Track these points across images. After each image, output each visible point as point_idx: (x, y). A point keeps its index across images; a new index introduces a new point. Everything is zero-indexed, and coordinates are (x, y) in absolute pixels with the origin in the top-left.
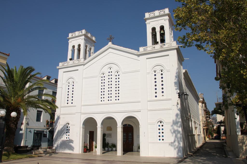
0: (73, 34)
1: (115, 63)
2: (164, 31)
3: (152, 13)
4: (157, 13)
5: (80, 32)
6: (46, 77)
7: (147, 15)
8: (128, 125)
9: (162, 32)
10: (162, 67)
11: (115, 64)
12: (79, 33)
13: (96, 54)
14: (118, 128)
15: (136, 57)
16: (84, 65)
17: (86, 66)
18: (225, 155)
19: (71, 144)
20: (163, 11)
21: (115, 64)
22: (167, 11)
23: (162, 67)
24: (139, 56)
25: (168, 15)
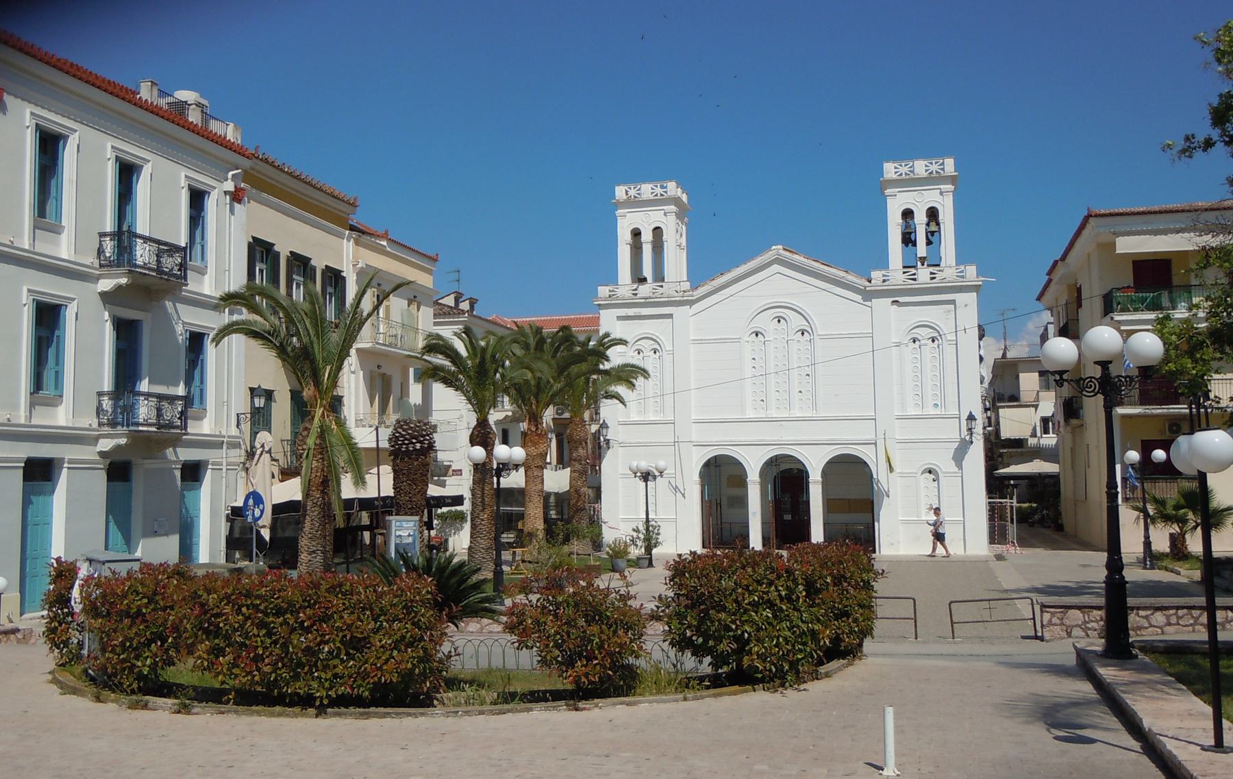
0: (630, 188)
1: (804, 310)
2: (938, 224)
3: (903, 164)
4: (921, 167)
5: (656, 186)
6: (468, 301)
7: (890, 170)
8: (796, 471)
9: (933, 228)
10: (809, 323)
11: (803, 316)
12: (652, 189)
13: (323, 200)
14: (1212, 727)
15: (858, 298)
16: (691, 303)
17: (697, 307)
18: (443, 513)
19: (456, 560)
20: (936, 163)
21: (803, 316)
22: (949, 166)
23: (809, 323)
24: (868, 295)
25: (952, 180)
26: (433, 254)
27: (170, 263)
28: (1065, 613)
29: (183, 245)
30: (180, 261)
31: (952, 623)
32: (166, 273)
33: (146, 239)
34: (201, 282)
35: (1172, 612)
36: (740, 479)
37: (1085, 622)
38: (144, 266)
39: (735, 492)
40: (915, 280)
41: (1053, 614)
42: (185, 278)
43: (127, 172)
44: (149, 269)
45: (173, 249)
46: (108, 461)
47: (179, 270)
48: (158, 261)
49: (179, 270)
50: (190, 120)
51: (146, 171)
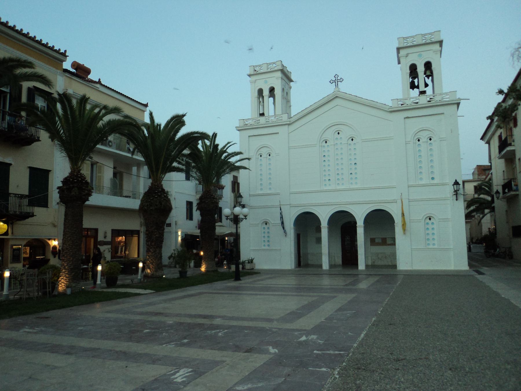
26: (145, 103)
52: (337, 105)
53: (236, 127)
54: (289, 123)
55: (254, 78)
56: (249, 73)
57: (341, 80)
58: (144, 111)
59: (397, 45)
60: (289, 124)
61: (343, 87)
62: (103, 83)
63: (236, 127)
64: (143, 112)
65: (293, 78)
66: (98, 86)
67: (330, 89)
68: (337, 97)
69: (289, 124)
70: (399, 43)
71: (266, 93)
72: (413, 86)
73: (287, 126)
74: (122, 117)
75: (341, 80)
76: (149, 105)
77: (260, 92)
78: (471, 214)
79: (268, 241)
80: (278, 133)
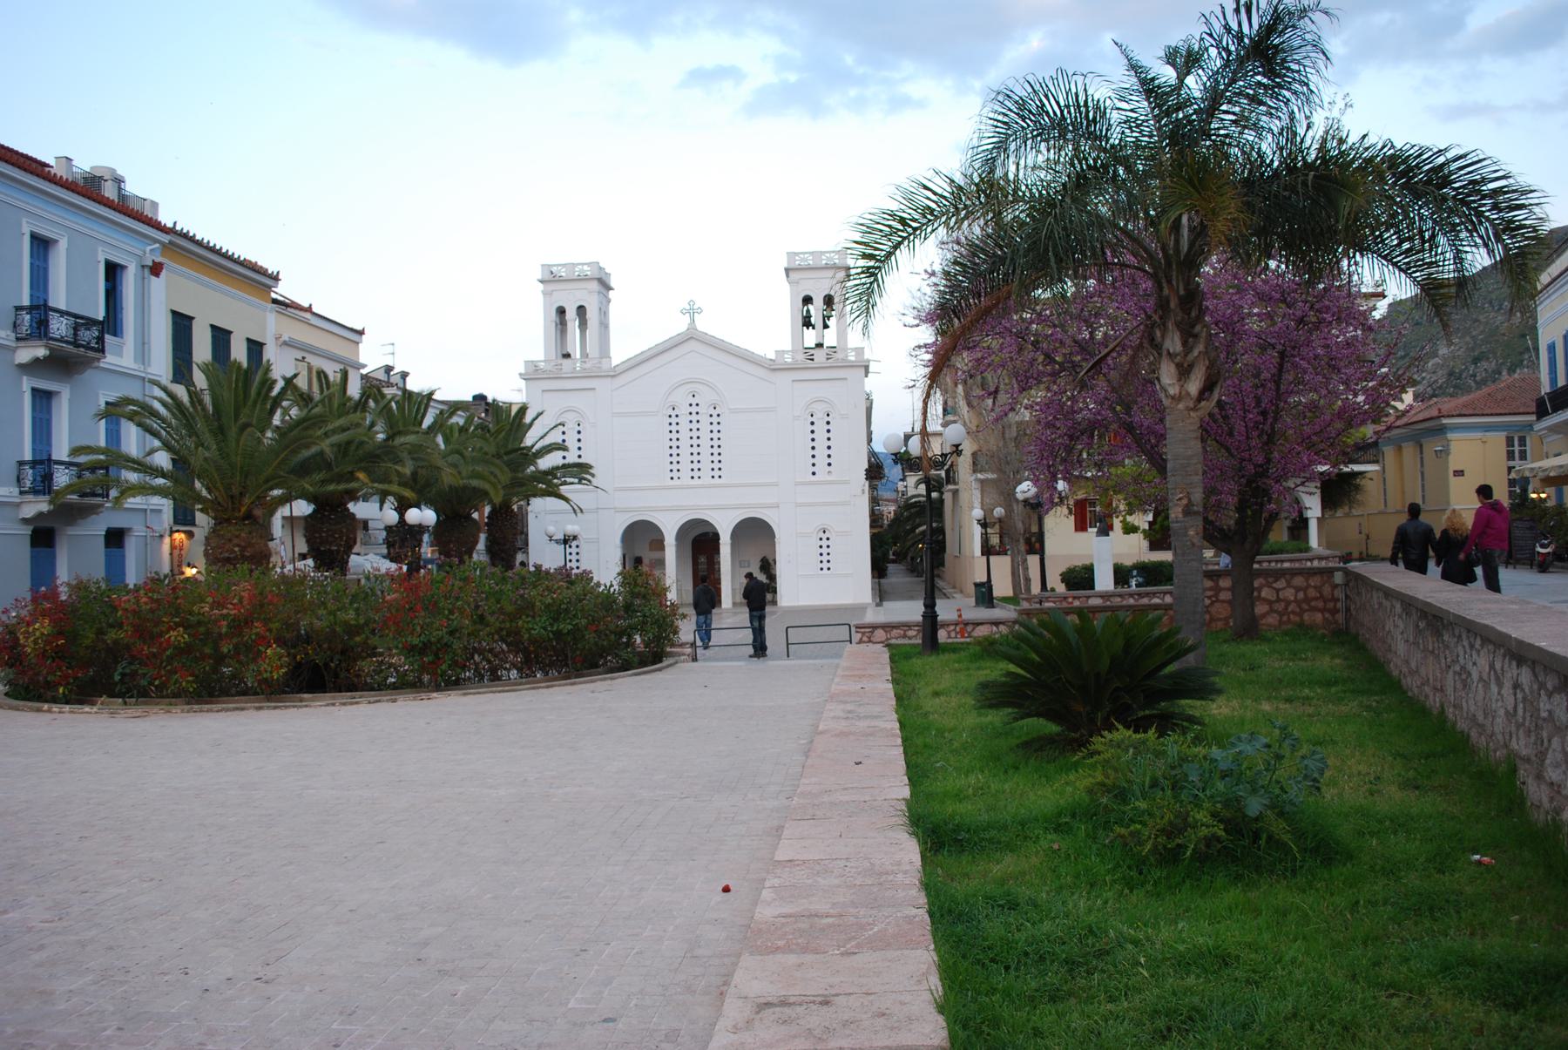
26: (359, 328)
27: (88, 335)
28: (872, 632)
29: (101, 319)
30: (1219, 66)
31: (788, 644)
32: (83, 346)
33: (62, 313)
34: (120, 355)
35: (952, 628)
36: (659, 544)
37: (887, 639)
38: (61, 340)
39: (655, 555)
40: (812, 360)
41: (863, 633)
42: (102, 351)
43: (41, 245)
44: (67, 342)
45: (90, 322)
46: (31, 528)
47: (97, 343)
48: (75, 334)
49: (97, 343)
50: (106, 195)
51: (63, 245)
52: (691, 338)
53: (520, 374)
54: (612, 374)
55: (551, 287)
56: (540, 277)
57: (700, 311)
58: (358, 343)
59: (786, 265)
60: (613, 376)
61: (703, 325)
62: (314, 310)
63: (520, 374)
64: (353, 345)
65: (612, 284)
66: (308, 315)
67: (680, 325)
68: (691, 338)
69: (613, 376)
70: (788, 263)
71: (571, 314)
72: (807, 323)
73: (609, 379)
74: (1192, 720)
75: (700, 311)
76: (366, 331)
77: (561, 311)
78: (283, 493)
79: (578, 561)
80: (594, 389)
